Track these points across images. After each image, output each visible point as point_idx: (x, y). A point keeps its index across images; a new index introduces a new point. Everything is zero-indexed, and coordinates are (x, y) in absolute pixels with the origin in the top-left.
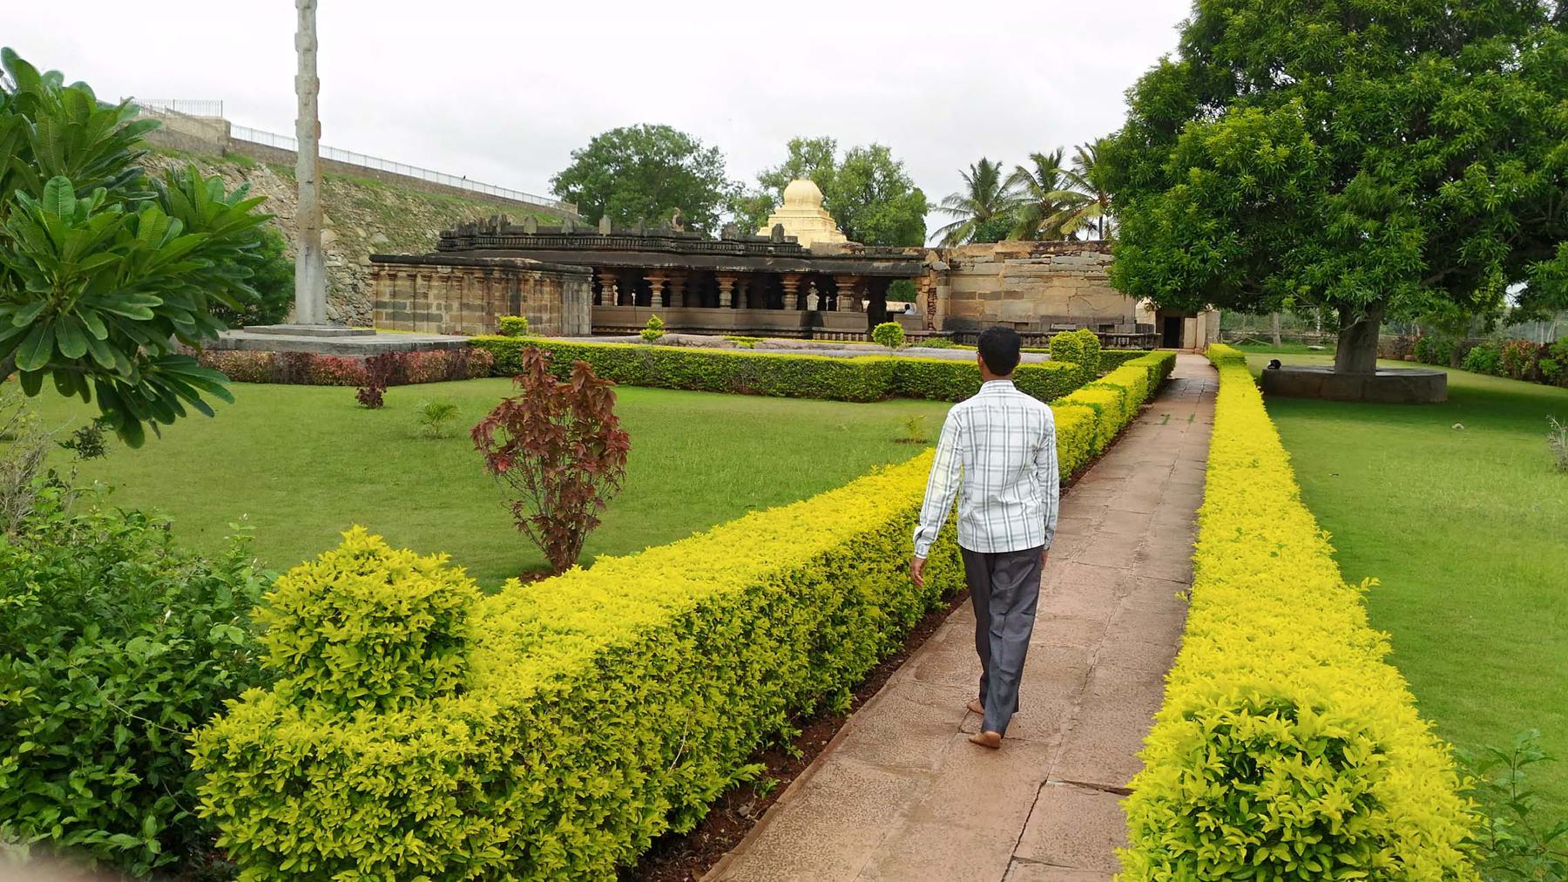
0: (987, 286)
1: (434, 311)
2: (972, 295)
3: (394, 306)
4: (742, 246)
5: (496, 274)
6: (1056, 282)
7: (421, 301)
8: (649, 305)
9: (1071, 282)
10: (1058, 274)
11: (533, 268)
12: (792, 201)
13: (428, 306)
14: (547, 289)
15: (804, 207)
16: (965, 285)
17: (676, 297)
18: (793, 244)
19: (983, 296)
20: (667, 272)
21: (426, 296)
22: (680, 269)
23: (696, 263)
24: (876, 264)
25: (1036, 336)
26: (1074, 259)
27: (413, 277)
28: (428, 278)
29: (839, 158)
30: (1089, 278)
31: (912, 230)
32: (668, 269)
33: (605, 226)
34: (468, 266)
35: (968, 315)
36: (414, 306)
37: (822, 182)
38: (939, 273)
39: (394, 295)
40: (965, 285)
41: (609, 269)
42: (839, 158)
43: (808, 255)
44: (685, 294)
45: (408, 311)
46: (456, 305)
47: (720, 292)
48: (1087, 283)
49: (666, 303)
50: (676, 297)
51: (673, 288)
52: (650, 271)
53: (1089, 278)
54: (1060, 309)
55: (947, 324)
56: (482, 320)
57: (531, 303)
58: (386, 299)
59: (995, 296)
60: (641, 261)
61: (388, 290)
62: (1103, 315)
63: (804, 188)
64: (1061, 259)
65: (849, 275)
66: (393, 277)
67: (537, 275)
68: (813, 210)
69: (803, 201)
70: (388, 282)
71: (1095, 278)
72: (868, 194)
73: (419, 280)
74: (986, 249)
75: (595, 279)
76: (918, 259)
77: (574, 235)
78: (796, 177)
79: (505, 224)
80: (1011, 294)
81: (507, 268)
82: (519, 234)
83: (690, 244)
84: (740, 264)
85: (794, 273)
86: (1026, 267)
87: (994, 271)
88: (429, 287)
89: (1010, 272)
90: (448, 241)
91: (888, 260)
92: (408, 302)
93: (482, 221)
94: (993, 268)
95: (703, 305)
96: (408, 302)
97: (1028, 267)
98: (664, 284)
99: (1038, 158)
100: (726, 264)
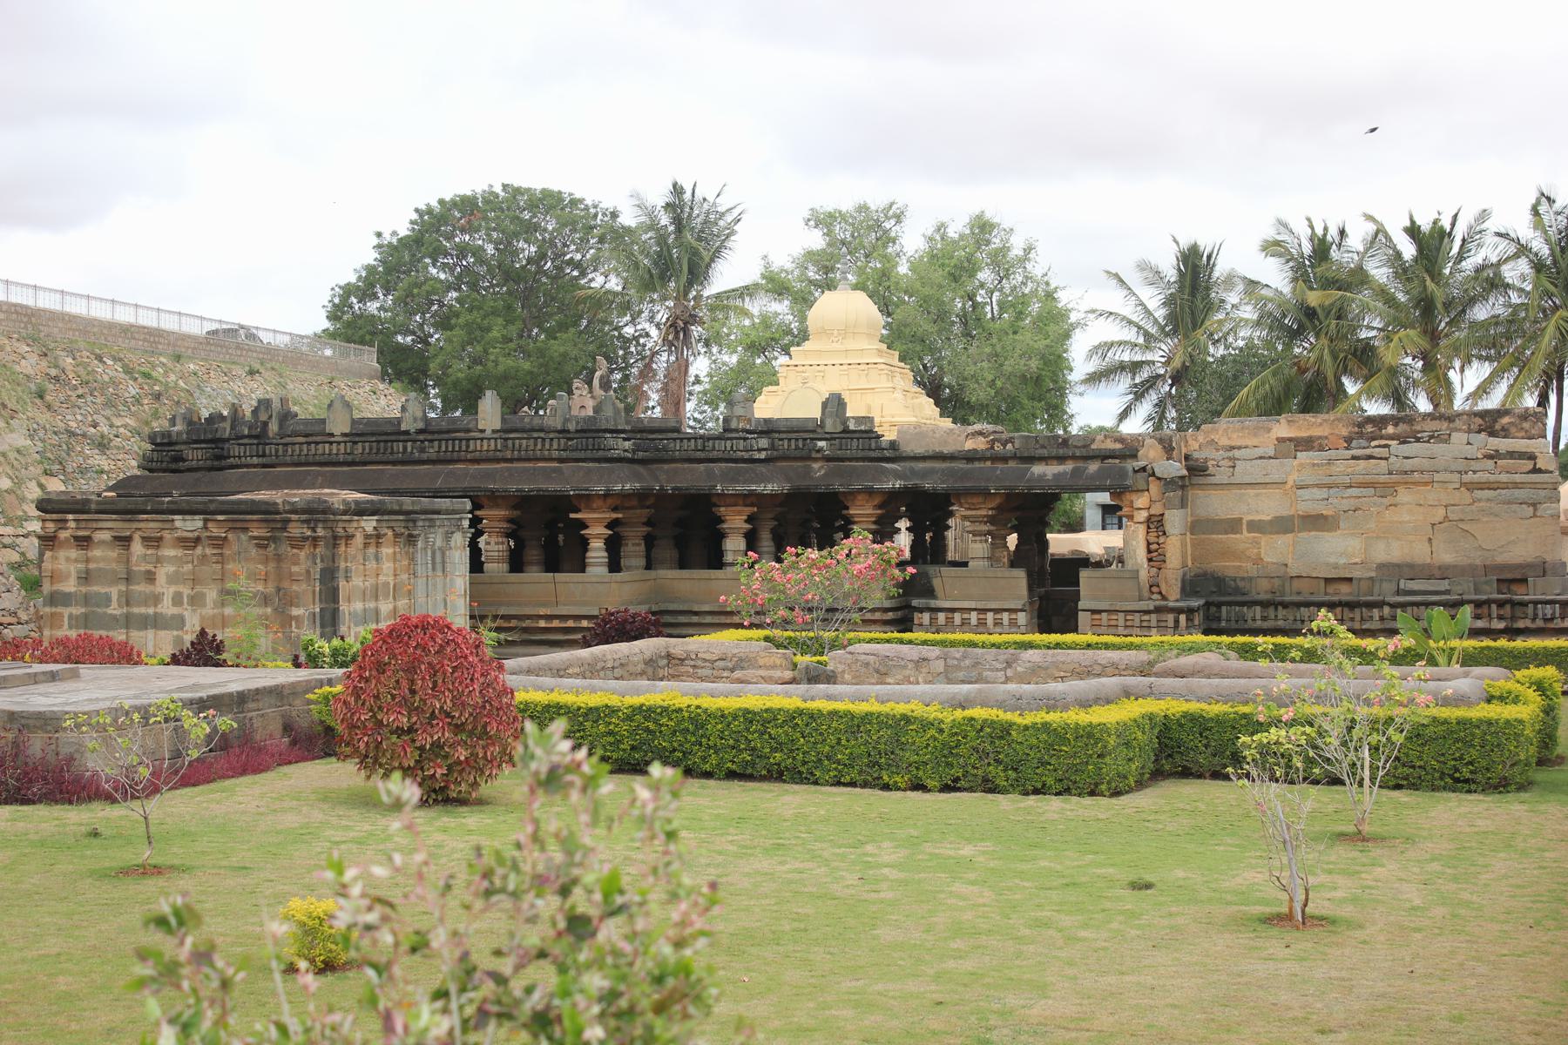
0: (1267, 506)
1: (167, 608)
2: (1233, 526)
3: (86, 600)
4: (764, 443)
5: (296, 530)
6: (1404, 496)
7: (140, 588)
8: (582, 568)
9: (1432, 495)
10: (1407, 477)
11: (361, 511)
12: (825, 332)
13: (157, 599)
14: (387, 551)
15: (851, 344)
16: (1214, 504)
17: (633, 552)
18: (868, 434)
19: (1254, 526)
20: (619, 501)
21: (150, 577)
22: (641, 497)
23: (668, 479)
24: (1038, 469)
25: (1371, 605)
26: (1437, 448)
27: (124, 541)
28: (153, 542)
29: (912, 241)
30: (1471, 487)
31: (1045, 386)
32: (623, 495)
33: (490, 412)
34: (240, 514)
35: (1227, 567)
36: (128, 600)
37: (882, 290)
38: (1170, 484)
39: (86, 578)
40: (1214, 504)
41: (495, 498)
42: (912, 241)
43: (894, 453)
44: (649, 541)
45: (114, 609)
46: (211, 594)
47: (722, 536)
48: (1466, 496)
49: (614, 566)
50: (633, 552)
51: (625, 531)
52: (586, 499)
53: (1471, 487)
54: (1412, 549)
55: (1190, 586)
56: (265, 623)
57: (357, 581)
58: (70, 586)
59: (1282, 525)
60: (566, 480)
61: (73, 569)
62: (1501, 559)
63: (846, 308)
64: (1412, 448)
65: (985, 494)
66: (84, 542)
67: (369, 524)
68: (870, 348)
69: (848, 331)
70: (74, 553)
71: (1482, 486)
72: (961, 313)
73: (137, 547)
74: (1255, 432)
75: (475, 522)
76: (1122, 456)
77: (428, 431)
78: (830, 286)
79: (286, 416)
80: (1317, 522)
81: (316, 513)
82: (315, 432)
83: (658, 443)
84: (765, 480)
85: (870, 492)
86: (1340, 467)
87: (1275, 477)
88: (159, 560)
89: (1309, 477)
90: (167, 455)
91: (1061, 459)
92: (114, 592)
93: (235, 409)
94: (1276, 470)
95: (683, 564)
96: (114, 592)
97: (1344, 467)
98: (611, 525)
99: (1413, 231)
100: (735, 480)
